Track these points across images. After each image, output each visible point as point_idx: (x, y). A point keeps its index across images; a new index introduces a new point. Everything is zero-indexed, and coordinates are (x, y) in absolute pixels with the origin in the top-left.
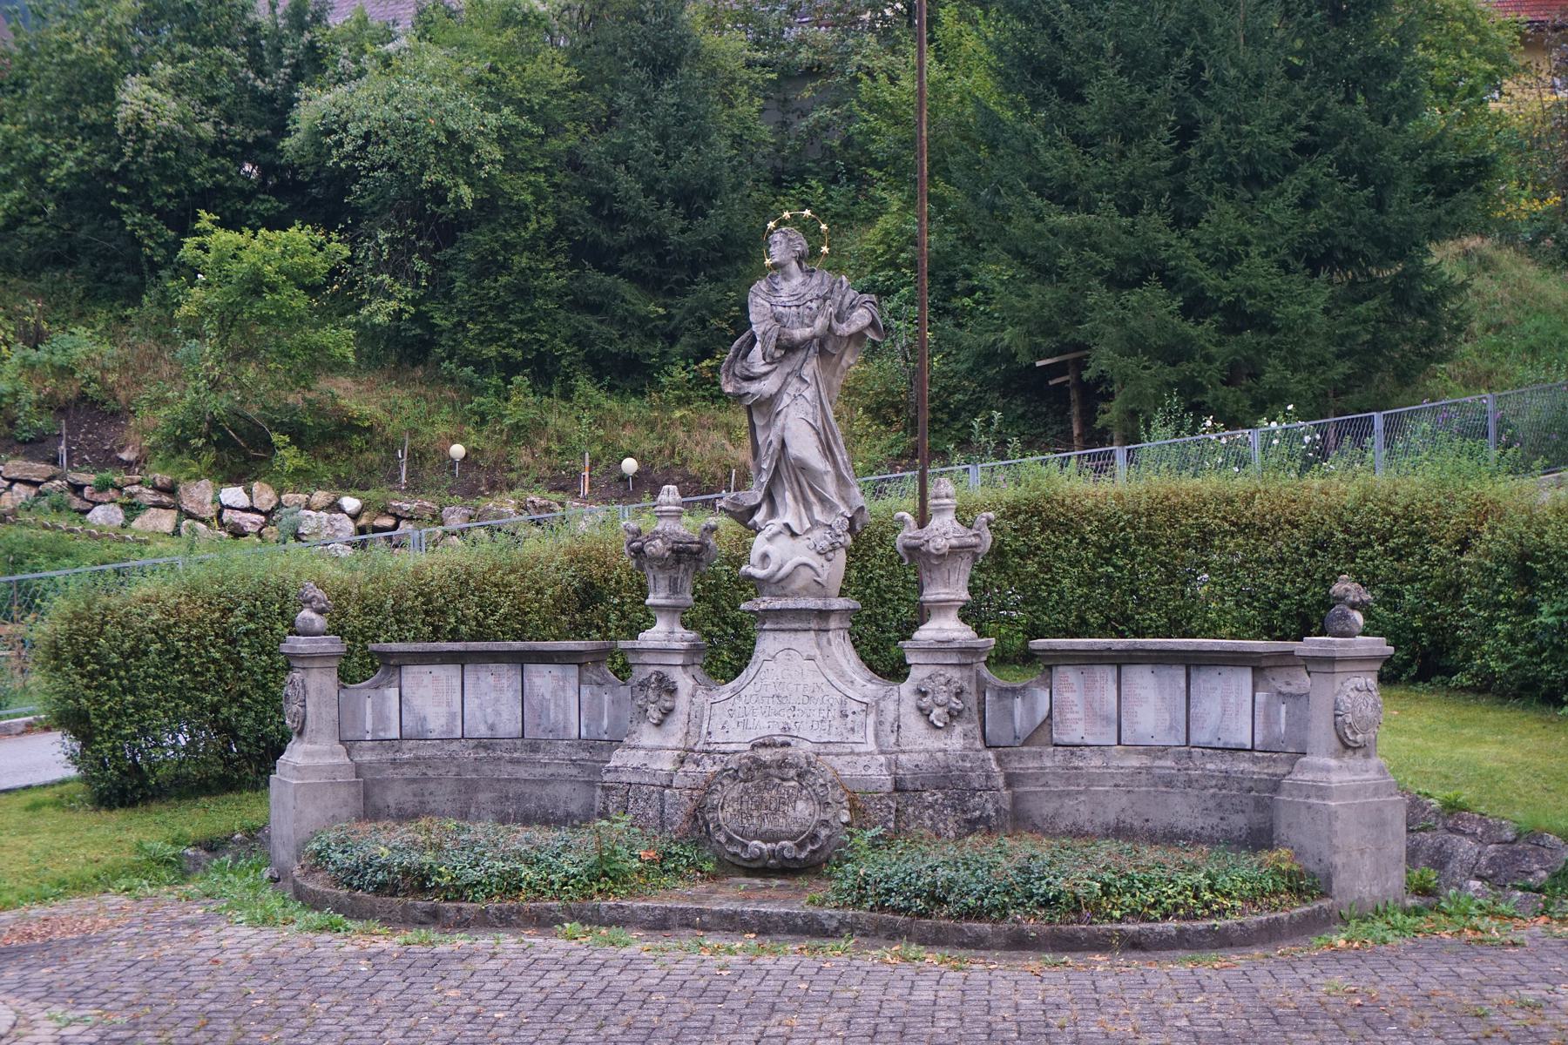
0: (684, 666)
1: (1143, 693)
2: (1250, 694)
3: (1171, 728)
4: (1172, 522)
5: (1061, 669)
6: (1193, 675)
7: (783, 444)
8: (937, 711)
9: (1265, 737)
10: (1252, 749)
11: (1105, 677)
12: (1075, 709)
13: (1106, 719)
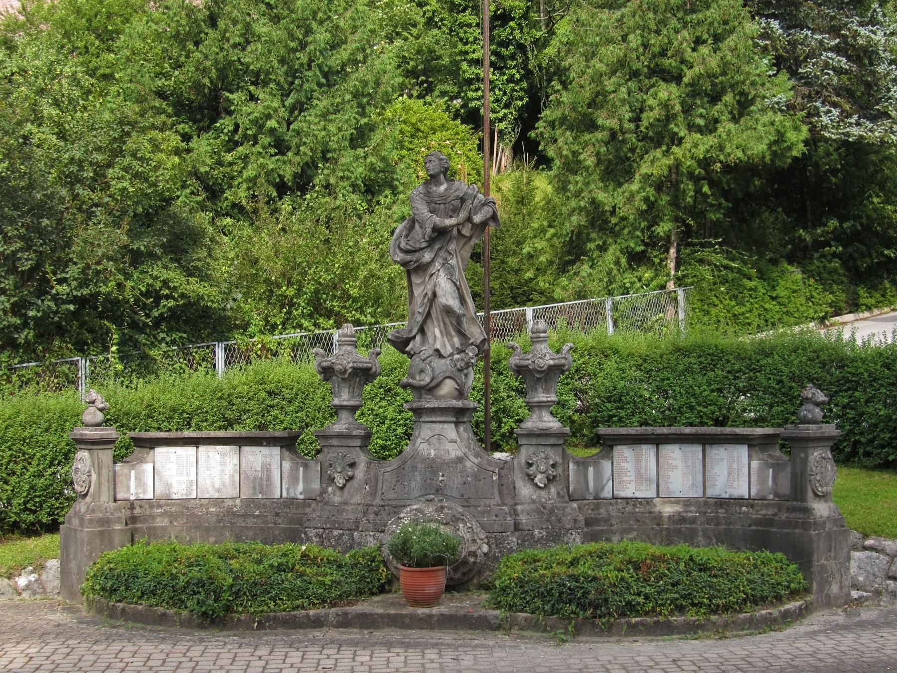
0: (360, 447)
1: (624, 465)
2: (747, 462)
3: (693, 485)
4: (827, 350)
5: (619, 447)
6: (707, 451)
7: (435, 295)
8: (539, 476)
9: (759, 491)
10: (750, 498)
11: (648, 452)
12: (628, 474)
13: (649, 480)
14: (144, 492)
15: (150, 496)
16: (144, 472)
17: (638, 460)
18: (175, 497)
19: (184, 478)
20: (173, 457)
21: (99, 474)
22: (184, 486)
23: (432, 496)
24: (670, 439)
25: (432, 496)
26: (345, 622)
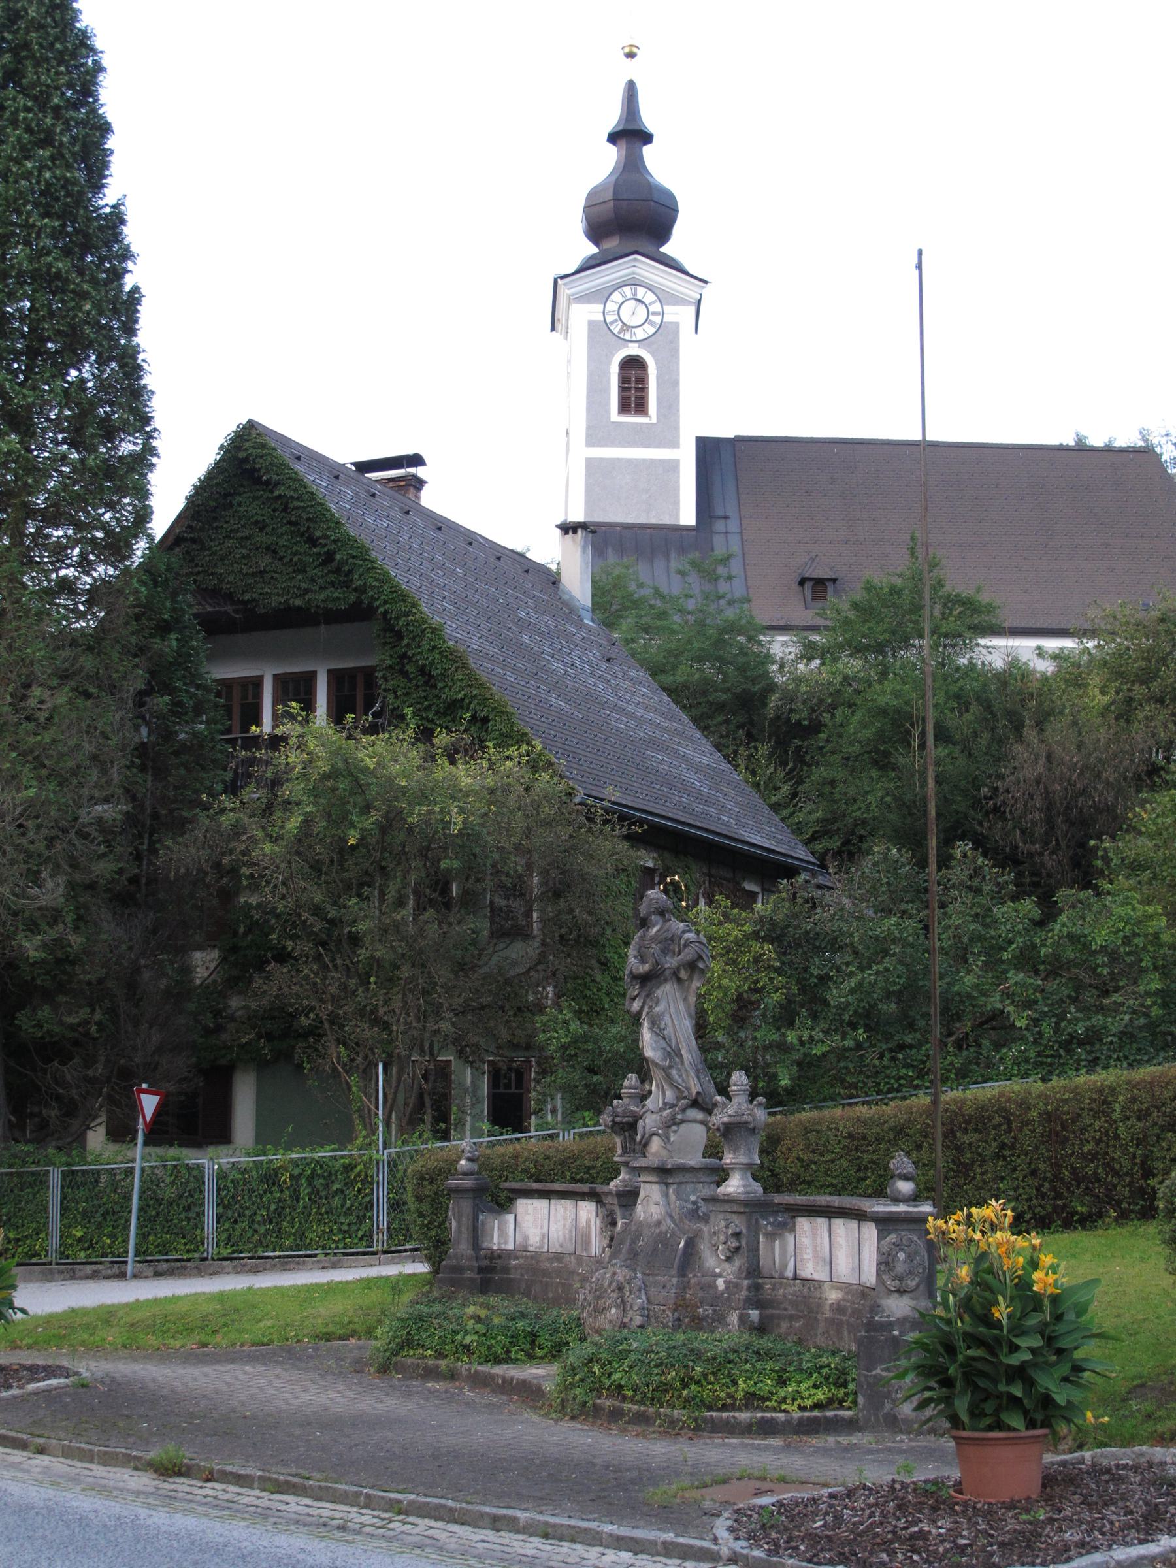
6: (833, 1227)
14: (506, 1243)
15: (511, 1246)
16: (506, 1222)
17: (814, 1235)
18: (531, 1249)
19: (538, 1231)
20: (530, 1208)
21: (459, 1223)
22: (538, 1239)
23: (297, 1226)
24: (807, 1211)
25: (297, 1226)
26: (481, 1382)
